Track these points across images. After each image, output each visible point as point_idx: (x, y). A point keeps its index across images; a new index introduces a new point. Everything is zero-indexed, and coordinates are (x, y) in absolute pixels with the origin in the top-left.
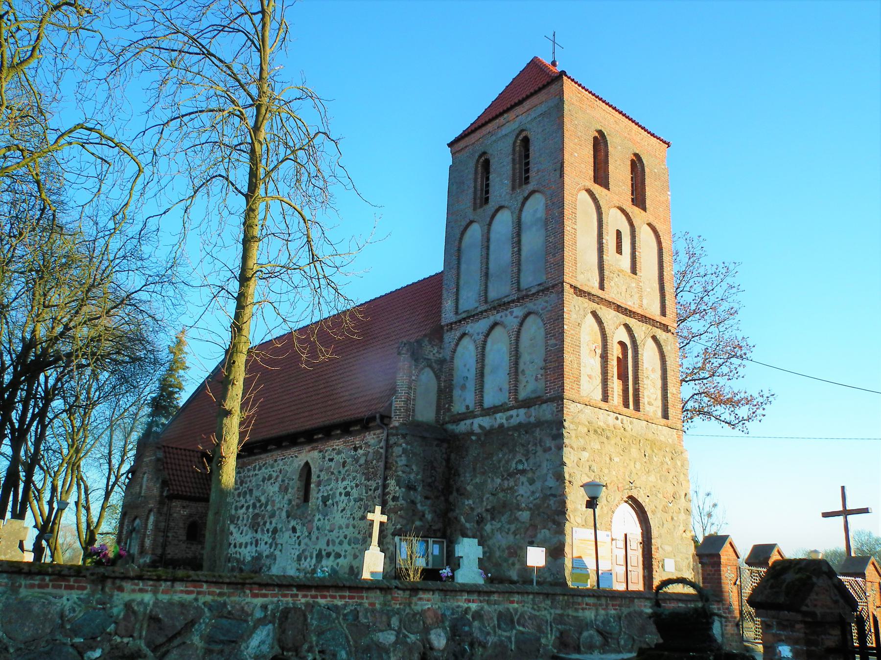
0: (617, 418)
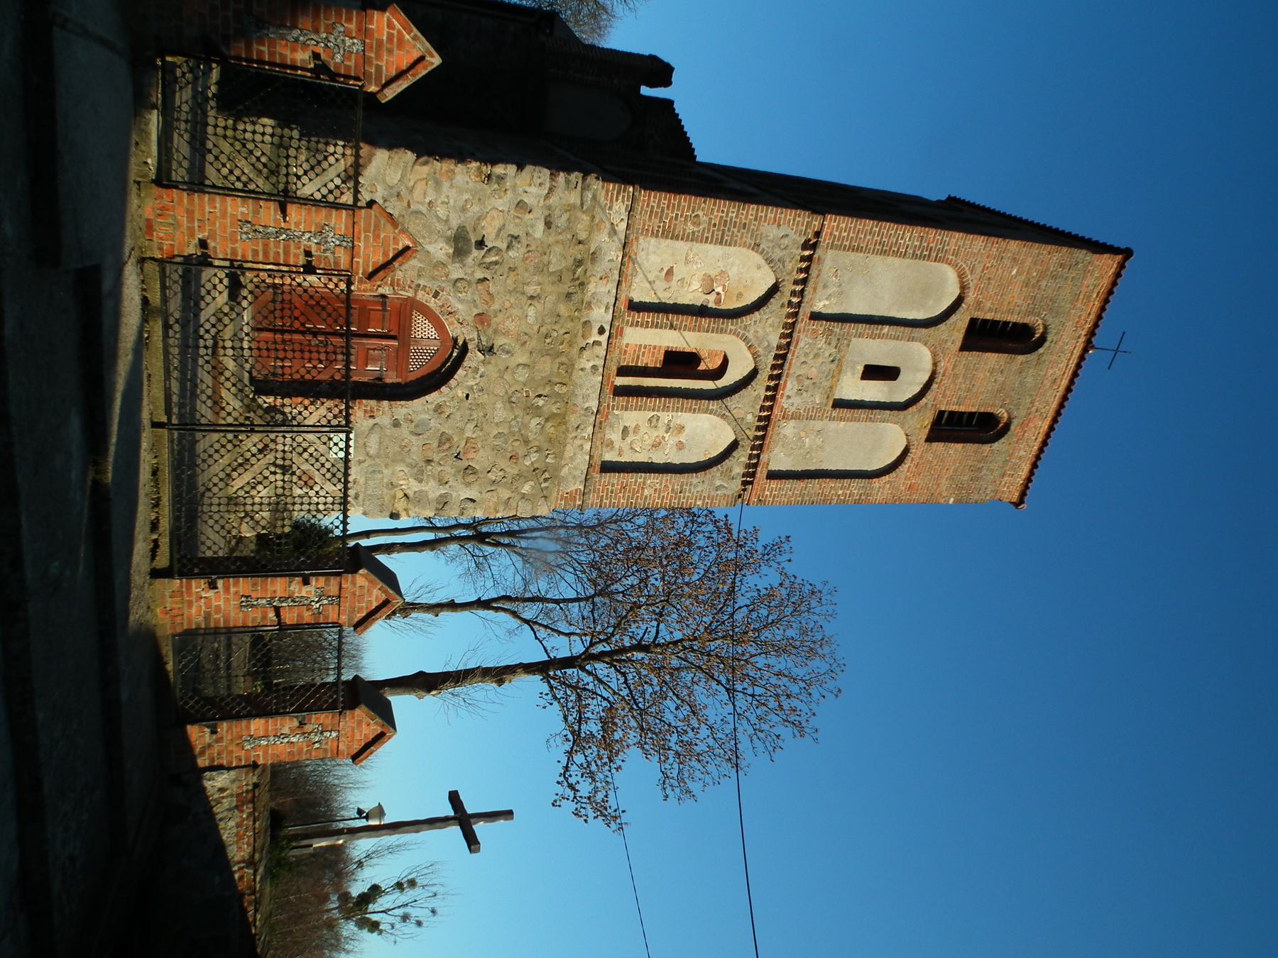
0: (601, 331)
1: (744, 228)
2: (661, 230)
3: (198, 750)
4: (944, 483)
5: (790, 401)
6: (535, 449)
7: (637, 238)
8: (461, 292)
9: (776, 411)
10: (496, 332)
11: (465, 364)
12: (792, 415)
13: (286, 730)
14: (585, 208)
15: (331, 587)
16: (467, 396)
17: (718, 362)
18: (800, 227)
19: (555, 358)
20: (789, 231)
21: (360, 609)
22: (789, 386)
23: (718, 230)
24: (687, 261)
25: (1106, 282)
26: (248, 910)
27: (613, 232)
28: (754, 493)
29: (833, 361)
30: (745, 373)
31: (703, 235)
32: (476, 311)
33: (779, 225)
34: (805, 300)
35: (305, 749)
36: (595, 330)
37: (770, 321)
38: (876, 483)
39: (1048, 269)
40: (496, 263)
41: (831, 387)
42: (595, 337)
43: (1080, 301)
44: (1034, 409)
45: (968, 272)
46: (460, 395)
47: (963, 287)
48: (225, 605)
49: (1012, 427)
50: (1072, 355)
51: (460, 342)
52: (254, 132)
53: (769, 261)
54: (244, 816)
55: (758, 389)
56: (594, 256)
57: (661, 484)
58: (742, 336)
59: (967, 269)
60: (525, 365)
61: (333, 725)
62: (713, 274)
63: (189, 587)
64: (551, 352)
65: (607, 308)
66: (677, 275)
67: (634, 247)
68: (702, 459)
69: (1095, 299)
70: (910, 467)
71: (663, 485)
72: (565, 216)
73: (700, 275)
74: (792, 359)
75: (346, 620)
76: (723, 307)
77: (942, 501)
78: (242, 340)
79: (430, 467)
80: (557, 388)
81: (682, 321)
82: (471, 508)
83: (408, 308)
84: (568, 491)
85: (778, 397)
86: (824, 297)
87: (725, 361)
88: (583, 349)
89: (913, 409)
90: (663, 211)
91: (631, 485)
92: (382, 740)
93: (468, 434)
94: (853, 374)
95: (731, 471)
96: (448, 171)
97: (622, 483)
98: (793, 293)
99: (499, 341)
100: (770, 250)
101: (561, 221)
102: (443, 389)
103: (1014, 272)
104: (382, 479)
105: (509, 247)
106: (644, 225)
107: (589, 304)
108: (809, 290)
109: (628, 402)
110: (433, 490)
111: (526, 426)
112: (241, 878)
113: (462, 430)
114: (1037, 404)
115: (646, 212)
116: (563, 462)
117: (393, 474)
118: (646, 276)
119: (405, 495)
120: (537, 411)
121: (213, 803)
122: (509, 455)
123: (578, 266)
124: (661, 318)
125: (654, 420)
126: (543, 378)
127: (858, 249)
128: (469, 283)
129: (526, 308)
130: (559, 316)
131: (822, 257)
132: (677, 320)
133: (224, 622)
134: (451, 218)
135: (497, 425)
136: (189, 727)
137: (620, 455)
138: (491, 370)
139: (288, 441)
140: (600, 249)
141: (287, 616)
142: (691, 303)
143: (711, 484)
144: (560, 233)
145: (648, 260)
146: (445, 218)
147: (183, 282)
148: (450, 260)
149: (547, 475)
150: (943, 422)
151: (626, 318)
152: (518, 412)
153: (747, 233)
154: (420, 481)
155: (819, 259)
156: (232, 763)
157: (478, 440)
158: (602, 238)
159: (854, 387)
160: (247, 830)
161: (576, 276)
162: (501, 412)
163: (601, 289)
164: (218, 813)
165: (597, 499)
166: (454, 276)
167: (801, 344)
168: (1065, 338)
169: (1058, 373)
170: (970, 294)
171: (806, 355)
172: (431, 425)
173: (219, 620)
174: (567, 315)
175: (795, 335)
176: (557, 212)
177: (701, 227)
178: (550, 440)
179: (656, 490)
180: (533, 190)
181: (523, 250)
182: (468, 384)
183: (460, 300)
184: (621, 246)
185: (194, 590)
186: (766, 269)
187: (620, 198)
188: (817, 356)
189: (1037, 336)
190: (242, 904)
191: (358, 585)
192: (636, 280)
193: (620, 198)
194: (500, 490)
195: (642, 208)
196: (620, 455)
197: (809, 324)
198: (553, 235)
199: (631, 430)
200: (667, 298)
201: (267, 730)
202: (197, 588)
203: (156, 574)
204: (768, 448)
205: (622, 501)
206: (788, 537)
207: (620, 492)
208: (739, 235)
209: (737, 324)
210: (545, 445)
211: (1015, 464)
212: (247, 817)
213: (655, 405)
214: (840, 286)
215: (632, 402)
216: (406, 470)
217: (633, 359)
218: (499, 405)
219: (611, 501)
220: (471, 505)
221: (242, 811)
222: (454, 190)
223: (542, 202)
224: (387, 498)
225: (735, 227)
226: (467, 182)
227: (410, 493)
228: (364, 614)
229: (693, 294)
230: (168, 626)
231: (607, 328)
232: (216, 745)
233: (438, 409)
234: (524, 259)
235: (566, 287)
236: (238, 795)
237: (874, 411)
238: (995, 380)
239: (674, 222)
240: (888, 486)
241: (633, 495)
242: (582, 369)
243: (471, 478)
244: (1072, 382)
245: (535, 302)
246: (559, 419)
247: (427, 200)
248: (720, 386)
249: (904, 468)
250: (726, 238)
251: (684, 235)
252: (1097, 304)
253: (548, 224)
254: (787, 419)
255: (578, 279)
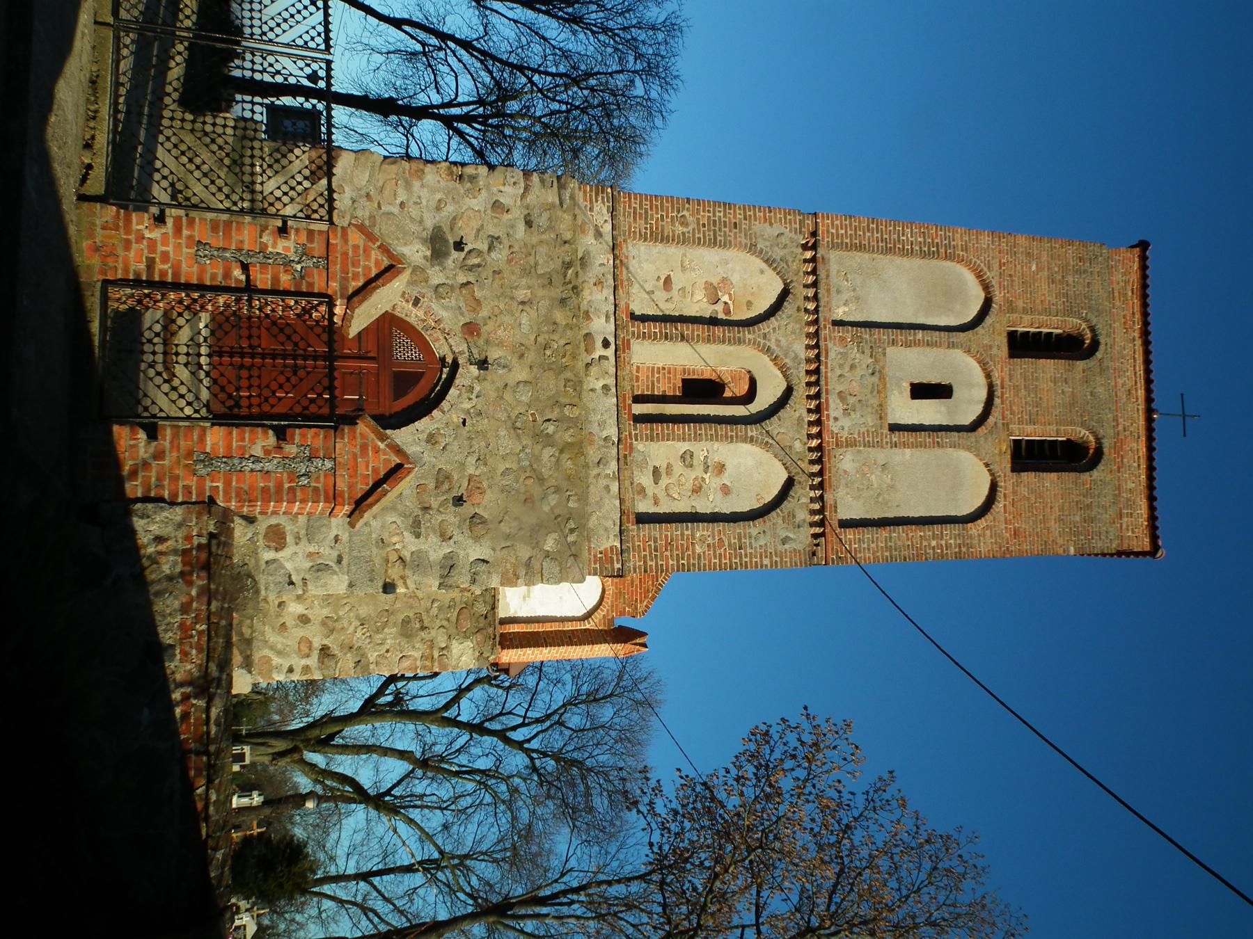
0: (606, 344)
1: (736, 227)
2: (648, 232)
3: (127, 468)
4: (1055, 527)
5: (839, 424)
6: (552, 489)
7: (625, 241)
8: (444, 299)
9: (826, 437)
10: (487, 342)
11: (457, 381)
12: (847, 441)
13: (257, 451)
14: (565, 206)
15: (315, 245)
16: (464, 423)
17: (745, 387)
18: (793, 225)
19: (560, 373)
20: (782, 230)
21: (356, 276)
22: (834, 408)
23: (709, 230)
24: (683, 268)
25: (1135, 277)
26: (197, 785)
27: (598, 234)
28: (829, 548)
29: (873, 374)
30: (779, 394)
31: (694, 235)
32: (463, 321)
33: (771, 224)
34: (822, 303)
35: (286, 486)
36: (599, 343)
37: (790, 328)
38: (974, 529)
39: (1068, 264)
40: (479, 266)
41: (881, 405)
42: (599, 351)
43: (1117, 299)
44: (1121, 428)
45: (986, 269)
46: (455, 420)
47: (986, 287)
48: (174, 251)
49: (1105, 450)
50: (1135, 361)
51: (449, 360)
52: (214, 125)
53: (769, 262)
54: (194, 593)
55: (799, 408)
56: (584, 262)
57: (714, 539)
58: (764, 347)
59: (982, 265)
60: (526, 382)
61: (326, 449)
62: (715, 281)
63: (128, 222)
64: (554, 366)
65: (607, 317)
66: (676, 286)
67: (624, 250)
68: (756, 505)
69: (1132, 298)
70: (1005, 506)
71: (717, 538)
72: (546, 215)
73: (701, 283)
74: (826, 372)
75: (338, 289)
76: (734, 317)
77: (1060, 551)
78: (199, 345)
79: (428, 516)
80: (567, 410)
81: (693, 331)
82: (484, 572)
83: (387, 326)
84: (602, 549)
85: (824, 418)
86: (842, 303)
87: (753, 383)
88: (588, 365)
89: (982, 430)
90: (646, 212)
91: (677, 540)
92: (399, 475)
93: (471, 470)
94: (901, 393)
95: (794, 516)
96: (417, 171)
97: (666, 536)
98: (809, 384)
99: (494, 354)
100: (768, 249)
101: (543, 221)
102: (435, 413)
103: (1034, 268)
104: (370, 533)
105: (491, 248)
106: (630, 227)
107: (587, 313)
108: (822, 292)
109: (652, 430)
110: (435, 550)
111: (537, 458)
112: (186, 715)
113: (462, 465)
114: (1121, 420)
115: (629, 213)
116: (589, 509)
117: (382, 527)
118: (642, 287)
119: (400, 558)
120: (548, 440)
121: (145, 562)
122: (523, 497)
123: (568, 268)
124: (668, 328)
125: (688, 457)
126: (549, 398)
127: (860, 248)
128: (452, 287)
129: (518, 314)
130: (555, 323)
131: (826, 256)
132: (688, 329)
133: (173, 274)
134: (425, 218)
135: (504, 458)
136: (116, 428)
137: (656, 503)
138: (489, 389)
139: (258, 59)
140: (588, 253)
141: (259, 276)
142: (698, 315)
143: (775, 535)
144: (542, 233)
145: (642, 269)
146: (418, 219)
147: (138, 393)
148: (428, 264)
149: (572, 525)
150: (1023, 454)
151: (631, 329)
152: (526, 441)
153: (740, 232)
154: (418, 536)
155: (823, 258)
156: (176, 495)
157: (482, 477)
158: (589, 240)
159: (909, 411)
160: (197, 620)
161: (568, 279)
162: (506, 442)
163: (598, 298)
164: (153, 582)
165: (640, 561)
166: (435, 281)
167: (832, 355)
168: (1120, 342)
169: (1130, 384)
170: (997, 293)
171: (841, 366)
172: (425, 460)
173: (167, 272)
174: (564, 323)
175: (822, 344)
176: (536, 211)
177: (690, 228)
178: (569, 478)
179: (709, 546)
180: (507, 189)
181: (506, 252)
182: (463, 406)
183: (445, 308)
184: (609, 249)
185: (135, 227)
186: (770, 273)
187: (600, 198)
188: (853, 367)
189: (1088, 342)
190: (185, 770)
191: (351, 243)
192: (634, 291)
193: (600, 198)
194: (519, 546)
195: (624, 209)
196: (656, 503)
197: (834, 331)
198: (535, 233)
199: (663, 470)
200: (669, 309)
201: (229, 447)
202: (138, 224)
203: (83, 198)
204: (830, 487)
205: (671, 562)
206: (891, 772)
207: (666, 550)
208: (732, 234)
209: (754, 332)
210: (565, 484)
211: (1128, 500)
212: (199, 595)
213: (684, 433)
214: (854, 290)
215: (657, 429)
216: (399, 522)
217: (648, 386)
218: (503, 433)
219: (657, 563)
220: (484, 567)
221: (190, 584)
222: (426, 190)
223: (519, 203)
224: (377, 561)
225: (725, 227)
226: (439, 182)
227: (406, 555)
228: (360, 284)
229: (698, 305)
230: (96, 269)
231: (612, 340)
232: (154, 463)
233: (431, 439)
234: (509, 261)
235: (557, 292)
236: (185, 553)
237: (940, 433)
238: (1063, 392)
239: (660, 223)
240: (988, 532)
241: (683, 553)
242: (592, 390)
243: (479, 529)
244: (1148, 391)
245: (527, 308)
246: (576, 449)
247: (398, 202)
248: (754, 411)
249: (999, 506)
250: (719, 238)
251: (674, 236)
252: (1137, 302)
253: (529, 223)
254: (842, 447)
255: (570, 282)
